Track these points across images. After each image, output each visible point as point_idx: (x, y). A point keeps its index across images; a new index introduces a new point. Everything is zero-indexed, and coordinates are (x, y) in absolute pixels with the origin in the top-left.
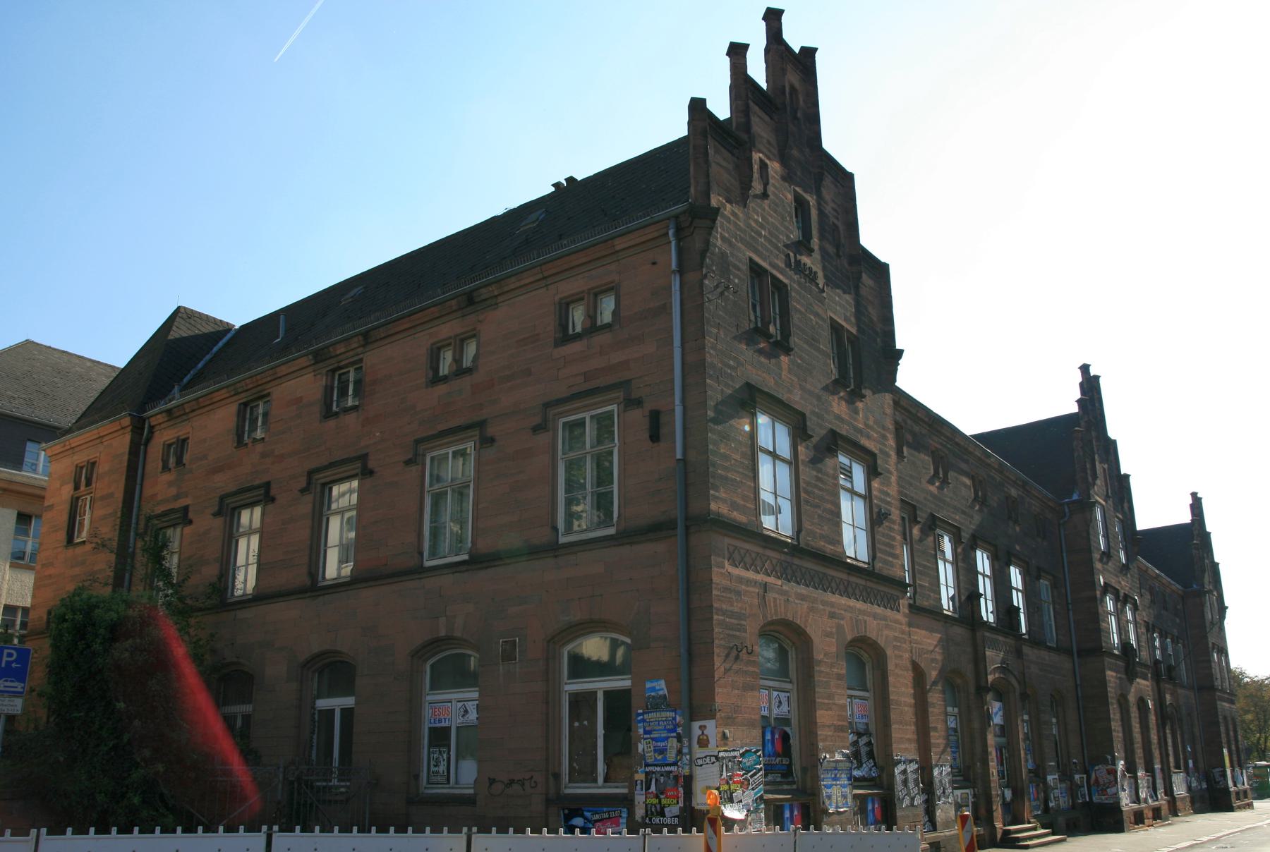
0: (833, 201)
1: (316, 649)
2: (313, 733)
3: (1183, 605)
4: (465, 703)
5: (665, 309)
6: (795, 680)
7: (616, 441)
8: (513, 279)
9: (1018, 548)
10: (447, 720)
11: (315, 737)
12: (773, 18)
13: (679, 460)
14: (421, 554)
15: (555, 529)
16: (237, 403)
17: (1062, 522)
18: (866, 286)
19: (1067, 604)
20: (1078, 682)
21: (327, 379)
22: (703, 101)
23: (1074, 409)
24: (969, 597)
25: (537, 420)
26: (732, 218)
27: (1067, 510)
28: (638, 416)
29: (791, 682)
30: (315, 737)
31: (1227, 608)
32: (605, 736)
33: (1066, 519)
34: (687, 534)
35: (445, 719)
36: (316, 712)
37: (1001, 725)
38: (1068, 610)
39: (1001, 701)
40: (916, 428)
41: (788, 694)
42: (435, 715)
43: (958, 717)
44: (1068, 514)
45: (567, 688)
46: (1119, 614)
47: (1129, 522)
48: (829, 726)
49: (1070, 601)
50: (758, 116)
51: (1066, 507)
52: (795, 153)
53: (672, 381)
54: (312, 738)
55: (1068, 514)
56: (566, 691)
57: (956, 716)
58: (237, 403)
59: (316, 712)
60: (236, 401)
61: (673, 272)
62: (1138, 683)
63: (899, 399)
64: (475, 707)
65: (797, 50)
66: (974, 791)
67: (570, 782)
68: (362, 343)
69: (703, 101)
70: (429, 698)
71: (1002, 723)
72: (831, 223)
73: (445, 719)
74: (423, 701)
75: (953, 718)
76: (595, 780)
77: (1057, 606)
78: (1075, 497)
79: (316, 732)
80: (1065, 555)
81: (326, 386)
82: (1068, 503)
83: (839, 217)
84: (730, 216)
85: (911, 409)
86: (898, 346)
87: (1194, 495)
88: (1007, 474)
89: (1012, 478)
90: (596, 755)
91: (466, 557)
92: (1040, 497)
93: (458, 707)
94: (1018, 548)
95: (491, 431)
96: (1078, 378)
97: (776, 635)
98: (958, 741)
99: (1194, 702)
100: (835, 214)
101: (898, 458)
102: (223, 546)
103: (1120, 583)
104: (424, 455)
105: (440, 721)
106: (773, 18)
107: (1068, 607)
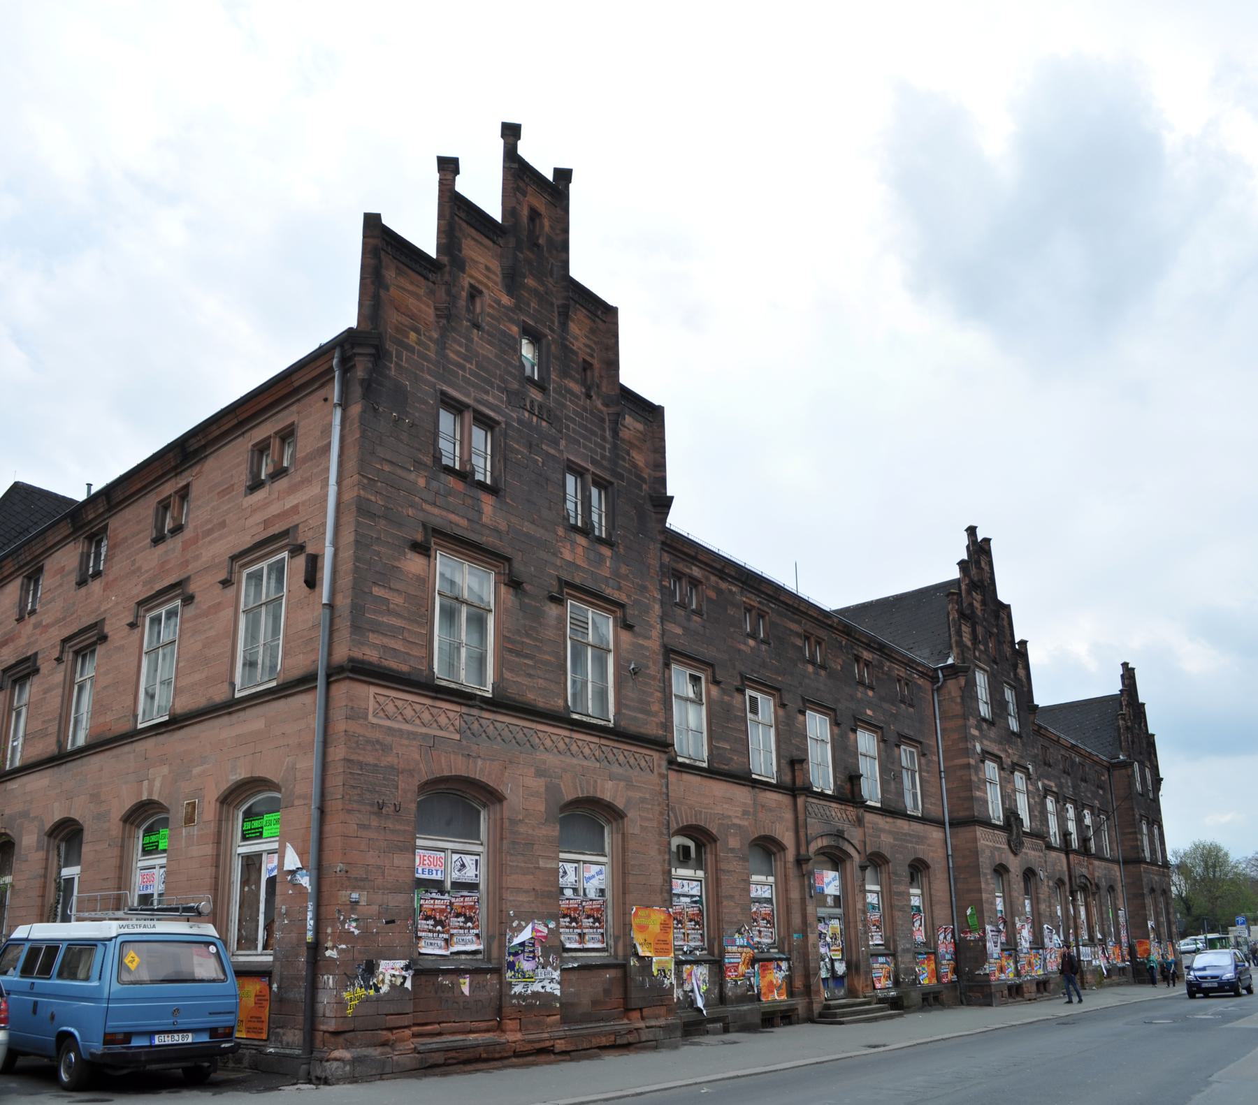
0: (586, 337)
1: (57, 817)
2: (58, 903)
3: (1109, 776)
4: (462, 856)
5: (327, 448)
6: (485, 843)
7: (285, 590)
8: (214, 427)
9: (869, 712)
10: (439, 872)
11: (60, 906)
12: (511, 132)
13: (325, 604)
14: (136, 716)
15: (233, 685)
16: (21, 577)
17: (935, 687)
18: (629, 429)
19: (940, 772)
20: (950, 853)
21: (83, 548)
22: (378, 216)
23: (954, 574)
24: (794, 761)
25: (223, 575)
26: (417, 347)
27: (941, 675)
28: (301, 561)
29: (482, 844)
30: (60, 906)
31: (1162, 779)
32: (266, 899)
33: (940, 684)
34: (328, 684)
35: (437, 871)
36: (62, 881)
37: (835, 896)
38: (941, 778)
39: (837, 870)
40: (724, 585)
41: (477, 857)
42: (424, 864)
43: (703, 882)
44: (941, 680)
45: (241, 850)
46: (1006, 783)
47: (1025, 689)
48: (527, 892)
49: (942, 769)
50: (473, 239)
51: (940, 672)
52: (530, 282)
53: (324, 524)
54: (56, 907)
55: (941, 680)
56: (239, 854)
57: (701, 881)
58: (21, 577)
59: (62, 881)
60: (20, 575)
61: (335, 405)
62: (1026, 854)
63: (697, 553)
64: (474, 862)
65: (550, 176)
66: (789, 964)
67: (238, 949)
68: (106, 507)
69: (378, 216)
70: (140, 864)
71: (838, 893)
72: (580, 360)
73: (437, 871)
74: (133, 868)
75: (875, 895)
76: (256, 948)
77: (924, 774)
78: (950, 661)
79: (61, 901)
80: (938, 721)
81: (82, 553)
82: (941, 668)
83: (595, 355)
84: (414, 345)
85: (714, 565)
86: (669, 494)
87: (1125, 665)
88: (857, 636)
89: (864, 640)
90: (258, 921)
91: (167, 718)
92: (905, 661)
93: (454, 859)
94: (869, 712)
95: (192, 588)
96: (964, 540)
97: (459, 793)
98: (773, 911)
99: (1118, 874)
100: (589, 351)
101: (516, 595)
102: (701, 776)
103: (1007, 751)
104: (144, 617)
105: (430, 872)
106: (511, 132)
107: (940, 775)
